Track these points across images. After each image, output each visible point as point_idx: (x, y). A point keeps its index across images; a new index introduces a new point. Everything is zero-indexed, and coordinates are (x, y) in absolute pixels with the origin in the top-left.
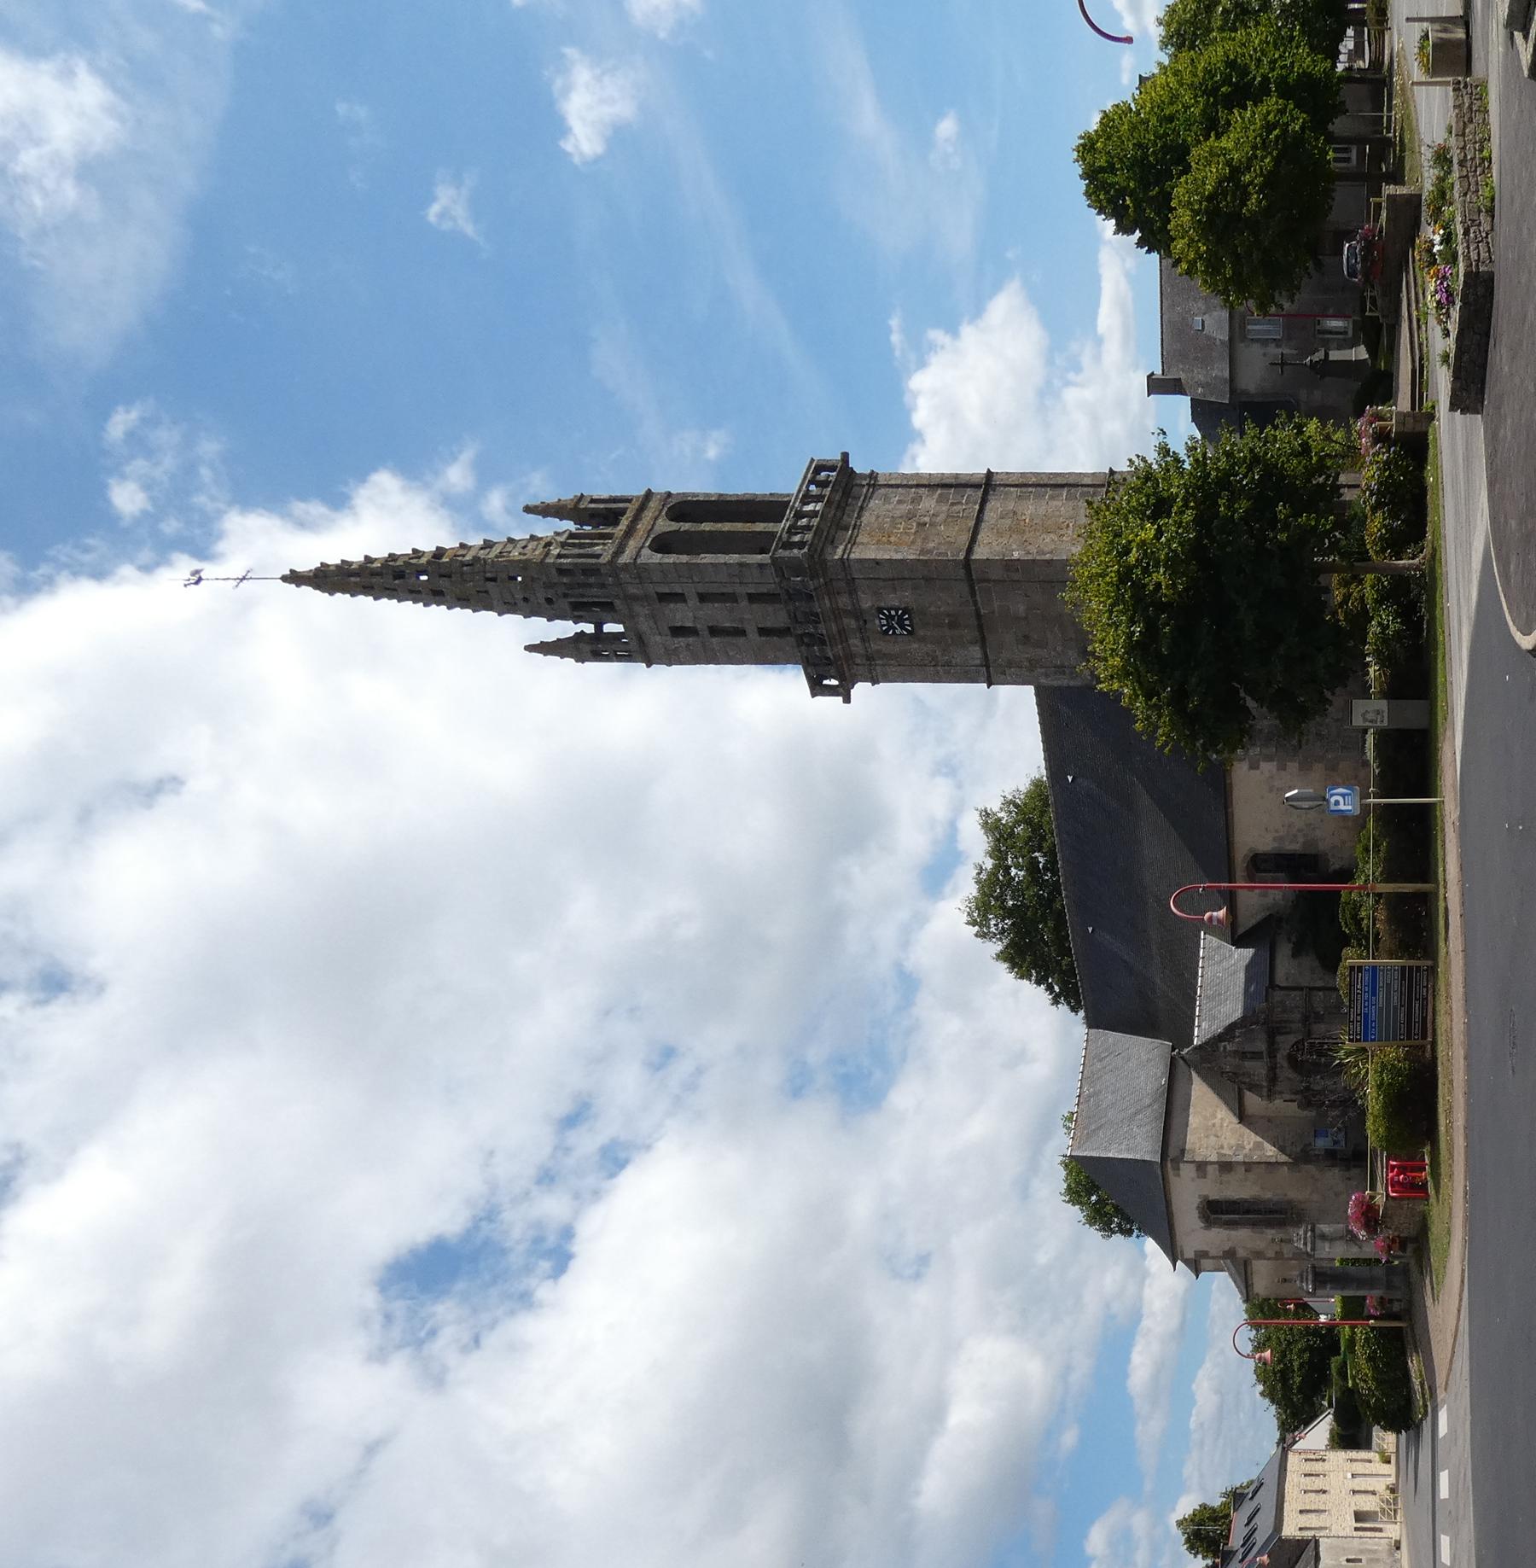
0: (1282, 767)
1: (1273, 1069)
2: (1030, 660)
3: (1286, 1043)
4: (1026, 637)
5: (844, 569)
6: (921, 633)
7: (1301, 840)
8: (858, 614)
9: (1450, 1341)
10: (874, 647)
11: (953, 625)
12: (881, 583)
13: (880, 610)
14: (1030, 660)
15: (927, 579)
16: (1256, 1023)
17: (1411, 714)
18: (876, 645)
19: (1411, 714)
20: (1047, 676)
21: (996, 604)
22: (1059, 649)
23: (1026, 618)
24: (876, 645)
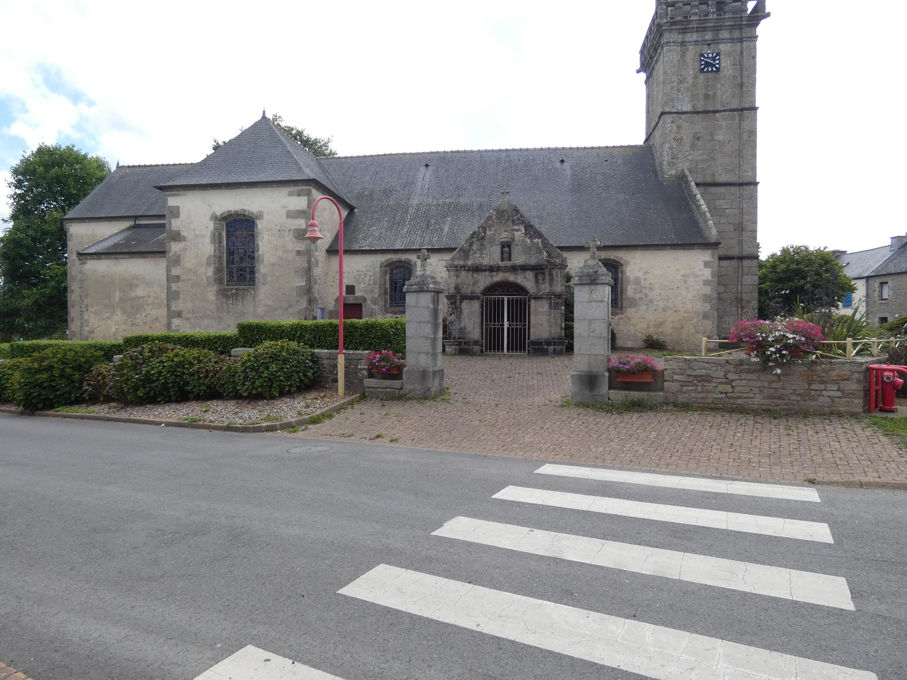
0: (706, 283)
1: (492, 269)
2: (681, 139)
3: (527, 281)
4: (698, 139)
5: (751, 37)
6: (701, 76)
7: (638, 296)
8: (716, 41)
9: (204, 181)
10: (691, 47)
11: (706, 96)
12: (738, 58)
13: (718, 54)
14: (681, 139)
15: (741, 85)
16: (549, 255)
17: (518, 325)
18: (692, 51)
19: (518, 325)
20: (671, 148)
21: (724, 123)
22: (690, 157)
23: (713, 139)
24: (692, 51)
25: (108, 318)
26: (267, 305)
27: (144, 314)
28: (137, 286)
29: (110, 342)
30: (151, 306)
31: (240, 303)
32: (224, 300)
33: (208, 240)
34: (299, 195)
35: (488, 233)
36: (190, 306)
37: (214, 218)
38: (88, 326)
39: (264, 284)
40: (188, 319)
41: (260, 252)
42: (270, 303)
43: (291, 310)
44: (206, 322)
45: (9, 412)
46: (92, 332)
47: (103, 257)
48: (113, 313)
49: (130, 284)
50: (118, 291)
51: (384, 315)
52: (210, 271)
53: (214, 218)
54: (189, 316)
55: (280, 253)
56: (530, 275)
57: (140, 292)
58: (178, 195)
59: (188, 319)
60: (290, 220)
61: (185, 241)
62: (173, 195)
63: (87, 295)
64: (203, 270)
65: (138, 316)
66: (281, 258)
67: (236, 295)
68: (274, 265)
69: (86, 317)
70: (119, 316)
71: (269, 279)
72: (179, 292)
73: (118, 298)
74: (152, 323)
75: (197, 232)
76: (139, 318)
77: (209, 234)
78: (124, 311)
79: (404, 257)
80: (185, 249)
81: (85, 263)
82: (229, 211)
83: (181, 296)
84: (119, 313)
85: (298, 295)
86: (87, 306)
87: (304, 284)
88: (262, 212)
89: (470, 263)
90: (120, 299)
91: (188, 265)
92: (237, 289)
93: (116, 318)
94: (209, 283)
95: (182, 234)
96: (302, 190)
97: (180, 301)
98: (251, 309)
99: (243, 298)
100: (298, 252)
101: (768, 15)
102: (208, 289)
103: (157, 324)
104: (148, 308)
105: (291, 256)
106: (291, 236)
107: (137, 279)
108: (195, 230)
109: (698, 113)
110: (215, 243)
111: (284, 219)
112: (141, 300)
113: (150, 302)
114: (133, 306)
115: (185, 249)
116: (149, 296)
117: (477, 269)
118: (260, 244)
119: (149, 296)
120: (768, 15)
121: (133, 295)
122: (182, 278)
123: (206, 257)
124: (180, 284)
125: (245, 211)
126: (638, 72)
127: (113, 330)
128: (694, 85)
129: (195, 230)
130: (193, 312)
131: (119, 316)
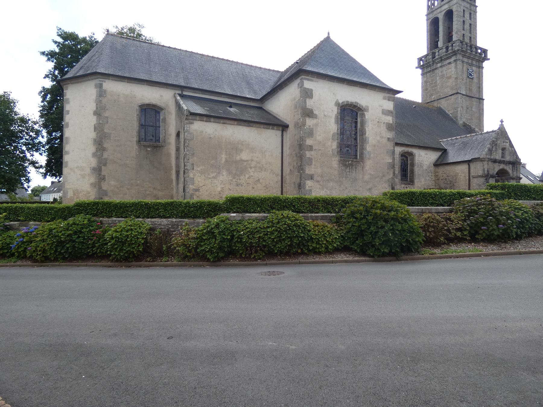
25: (214, 178)
26: (371, 174)
27: (247, 176)
28: (242, 150)
29: (215, 199)
30: (253, 169)
31: (354, 171)
32: (343, 168)
33: (333, 120)
34: (389, 100)
35: (498, 142)
36: (319, 171)
37: (337, 104)
38: (193, 184)
39: (369, 159)
40: (318, 181)
41: (367, 135)
42: (373, 173)
43: (384, 179)
44: (331, 184)
45: (346, 261)
46: (197, 190)
47: (212, 120)
48: (219, 173)
49: (235, 148)
50: (224, 153)
51: (400, 185)
52: (335, 145)
53: (337, 104)
54: (319, 179)
55: (378, 138)
56: (511, 166)
57: (244, 156)
58: (312, 80)
59: (318, 181)
60: (384, 116)
61: (316, 118)
62: (308, 80)
63: (193, 155)
64: (329, 143)
65: (242, 177)
66: (379, 142)
67: (352, 165)
68: (374, 146)
69: (191, 175)
70: (224, 176)
71: (372, 155)
72: (311, 159)
73: (224, 160)
74: (262, 183)
75: (326, 113)
76: (243, 179)
77: (334, 116)
78: (230, 173)
79: (410, 150)
80: (317, 125)
81: (192, 123)
82: (347, 101)
83: (314, 163)
84: (225, 173)
85: (388, 168)
86: (193, 164)
87: (391, 161)
88: (368, 107)
89: (492, 157)
90: (226, 161)
91: (319, 138)
92: (352, 161)
93: (221, 178)
94: (333, 154)
95: (315, 112)
96: (391, 97)
97: (313, 166)
98: (361, 176)
99: (356, 168)
100: (389, 139)
101: (489, 59)
102: (333, 159)
103: (259, 185)
104: (250, 171)
105: (385, 141)
106: (385, 128)
107: (242, 145)
108: (324, 111)
109: (468, 96)
110: (338, 123)
111: (380, 115)
112: (245, 164)
113: (252, 165)
114: (237, 168)
115: (317, 125)
116: (252, 160)
117: (495, 161)
118: (367, 129)
119: (252, 160)
120: (489, 59)
121: (238, 158)
122: (314, 148)
123: (332, 133)
124: (312, 153)
125: (358, 103)
126: (417, 68)
127: (219, 189)
128: (466, 83)
129: (324, 111)
130: (322, 176)
131: (224, 176)
